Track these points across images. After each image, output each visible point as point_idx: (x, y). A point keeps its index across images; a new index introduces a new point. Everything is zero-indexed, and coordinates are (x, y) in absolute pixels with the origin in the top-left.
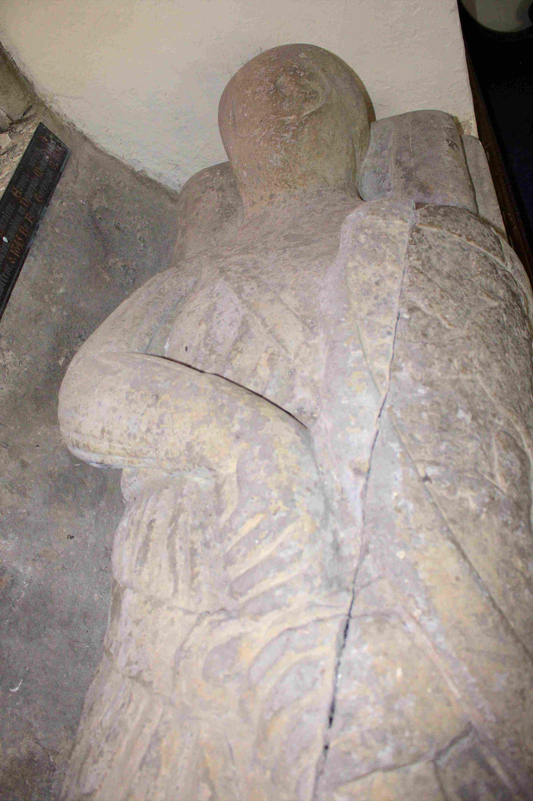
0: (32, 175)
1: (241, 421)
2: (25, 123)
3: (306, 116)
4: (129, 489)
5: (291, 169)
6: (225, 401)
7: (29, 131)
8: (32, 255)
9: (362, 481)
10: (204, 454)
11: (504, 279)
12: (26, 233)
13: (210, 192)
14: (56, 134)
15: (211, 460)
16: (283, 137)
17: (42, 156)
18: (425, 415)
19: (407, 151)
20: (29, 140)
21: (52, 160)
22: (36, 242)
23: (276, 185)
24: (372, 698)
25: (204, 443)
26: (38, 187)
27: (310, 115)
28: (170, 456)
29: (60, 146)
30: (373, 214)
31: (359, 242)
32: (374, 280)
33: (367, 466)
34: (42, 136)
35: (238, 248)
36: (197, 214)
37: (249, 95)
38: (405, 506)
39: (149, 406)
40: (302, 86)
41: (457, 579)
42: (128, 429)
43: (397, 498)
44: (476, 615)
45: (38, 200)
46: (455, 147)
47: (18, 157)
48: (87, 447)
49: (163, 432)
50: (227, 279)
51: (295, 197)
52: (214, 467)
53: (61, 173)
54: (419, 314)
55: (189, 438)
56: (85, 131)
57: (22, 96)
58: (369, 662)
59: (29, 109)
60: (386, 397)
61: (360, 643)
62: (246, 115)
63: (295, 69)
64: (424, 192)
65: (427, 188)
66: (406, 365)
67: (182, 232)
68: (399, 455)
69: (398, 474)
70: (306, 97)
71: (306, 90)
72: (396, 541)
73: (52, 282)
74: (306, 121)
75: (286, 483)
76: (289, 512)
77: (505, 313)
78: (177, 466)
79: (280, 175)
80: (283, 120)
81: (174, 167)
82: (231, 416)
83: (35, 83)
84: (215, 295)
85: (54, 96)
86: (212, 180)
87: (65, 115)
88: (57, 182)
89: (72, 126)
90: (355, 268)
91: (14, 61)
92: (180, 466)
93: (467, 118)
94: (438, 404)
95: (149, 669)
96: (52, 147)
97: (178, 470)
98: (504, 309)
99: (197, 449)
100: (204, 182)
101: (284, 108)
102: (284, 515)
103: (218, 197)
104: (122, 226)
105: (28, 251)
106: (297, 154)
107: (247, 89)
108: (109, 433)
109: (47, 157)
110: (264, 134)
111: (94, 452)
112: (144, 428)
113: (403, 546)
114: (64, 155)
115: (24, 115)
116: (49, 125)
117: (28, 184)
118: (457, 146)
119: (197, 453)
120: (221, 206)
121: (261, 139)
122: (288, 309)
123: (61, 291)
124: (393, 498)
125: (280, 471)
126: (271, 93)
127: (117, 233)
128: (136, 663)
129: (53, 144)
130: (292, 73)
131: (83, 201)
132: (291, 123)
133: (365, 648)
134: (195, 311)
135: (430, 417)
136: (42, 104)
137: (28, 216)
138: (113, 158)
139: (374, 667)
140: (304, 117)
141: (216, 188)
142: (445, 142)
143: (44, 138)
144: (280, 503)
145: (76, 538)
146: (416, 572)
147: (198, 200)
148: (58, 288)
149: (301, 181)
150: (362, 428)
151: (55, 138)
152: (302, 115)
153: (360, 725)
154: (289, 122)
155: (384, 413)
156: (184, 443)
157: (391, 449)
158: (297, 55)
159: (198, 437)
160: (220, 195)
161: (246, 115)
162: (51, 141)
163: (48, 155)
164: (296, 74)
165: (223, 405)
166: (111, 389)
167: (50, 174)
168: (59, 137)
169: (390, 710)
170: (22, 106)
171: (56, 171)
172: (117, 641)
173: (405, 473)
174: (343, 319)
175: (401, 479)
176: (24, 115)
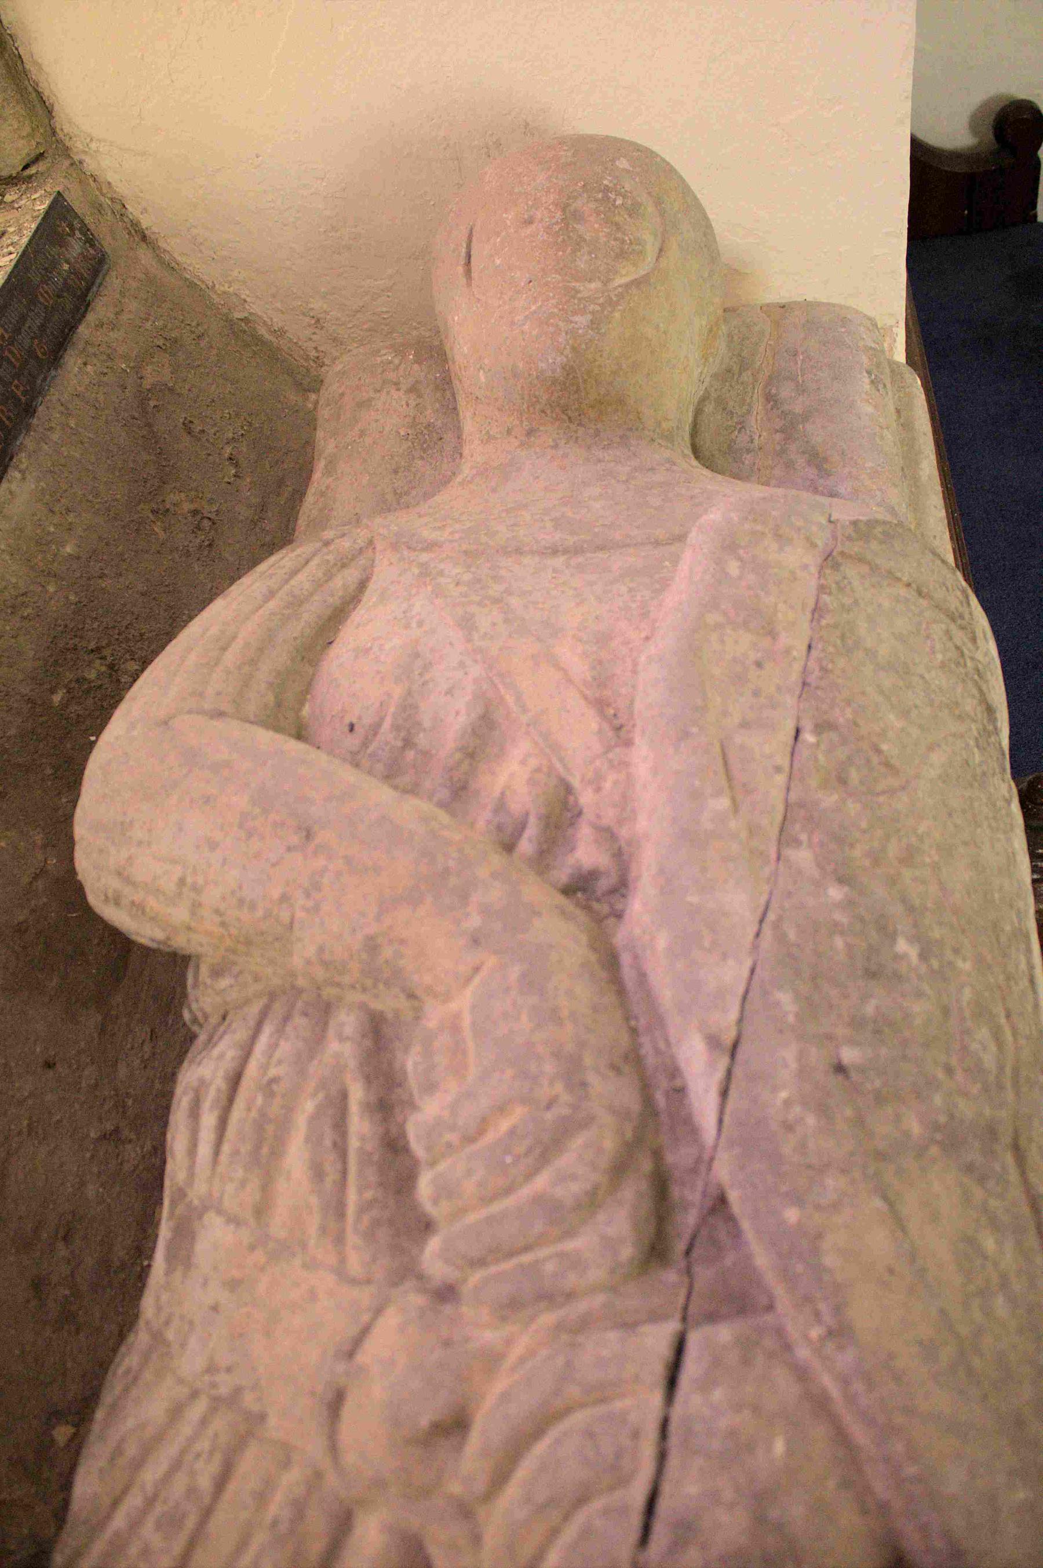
0: (33, 301)
1: (486, 911)
2: (24, 186)
3: (620, 286)
4: (204, 997)
5: (578, 387)
6: (451, 863)
7: (31, 206)
8: (17, 468)
9: (724, 1062)
10: (402, 963)
11: (976, 677)
12: (9, 418)
13: (393, 391)
14: (88, 220)
15: (416, 977)
16: (571, 322)
17: (54, 264)
18: (839, 942)
19: (792, 380)
20: (34, 226)
21: (75, 274)
22: (28, 441)
23: (543, 411)
24: (728, 1495)
25: (402, 942)
26: (43, 327)
27: (627, 286)
28: (327, 957)
29: (92, 246)
30: (755, 521)
31: (727, 574)
32: (753, 656)
33: (732, 1034)
34: (58, 219)
35: (457, 526)
36: (362, 434)
37: (508, 223)
38: (800, 1120)
39: (289, 849)
40: (618, 226)
41: (891, 1271)
42: (240, 887)
43: (787, 1103)
44: (921, 1343)
45: (40, 355)
46: (881, 387)
47: (8, 258)
48: (138, 908)
49: (317, 909)
50: (439, 592)
51: (576, 441)
52: (418, 993)
53: (88, 305)
54: (834, 736)
55: (373, 929)
56: (145, 222)
57: (28, 129)
58: (723, 1423)
59: (39, 157)
60: (770, 899)
61: (705, 1385)
62: (498, 262)
63: (606, 190)
64: (819, 468)
65: (826, 460)
66: (809, 839)
67: (326, 466)
68: (791, 1019)
69: (789, 1054)
70: (622, 250)
71: (624, 234)
72: (784, 1189)
73: (52, 529)
74: (621, 296)
75: (570, 1047)
76: (575, 1108)
77: (978, 747)
78: (338, 979)
79: (556, 395)
80: (574, 289)
81: (313, 322)
82: (464, 897)
83: (56, 108)
84: (414, 625)
85: (92, 140)
86: (397, 368)
87: (109, 183)
88: (80, 321)
89: (118, 207)
90: (719, 626)
91: (20, 57)
92: (346, 980)
93: (891, 322)
94: (862, 920)
95: (255, 1387)
96: (76, 247)
97: (338, 985)
98: (976, 739)
99: (387, 952)
100: (380, 370)
101: (578, 263)
102: (566, 1111)
103: (408, 405)
104: (197, 427)
105: (11, 459)
106: (595, 360)
107: (506, 211)
108: (196, 889)
109: (66, 267)
110: (534, 308)
111: (152, 919)
112: (276, 894)
113: (797, 1199)
114: (98, 265)
115: (25, 168)
116: (75, 200)
117: (23, 318)
118: (885, 386)
119: (387, 962)
120: (413, 424)
121: (526, 317)
122: (570, 681)
123: (69, 549)
124: (779, 1102)
125: (559, 1022)
126: (557, 228)
127: (186, 440)
128: (229, 1370)
129: (80, 239)
130: (600, 196)
131: (128, 366)
132: (589, 297)
133: (718, 1395)
134: (371, 648)
135: (849, 947)
136: (66, 152)
137: (17, 387)
138: (192, 285)
139: (732, 1433)
140: (615, 288)
141: (404, 387)
142: (865, 374)
143: (64, 224)
144: (559, 1087)
145: (61, 1069)
146: (815, 1251)
147: (364, 404)
148: (62, 544)
149: (592, 414)
150: (725, 956)
151: (85, 230)
152: (611, 286)
153: (704, 1547)
154: (585, 294)
155: (767, 932)
156: (360, 936)
157: (778, 1004)
158: (613, 161)
159: (391, 927)
160: (412, 403)
161: (498, 262)
162: (77, 233)
163: (68, 262)
164: (609, 198)
165: (447, 871)
166: (207, 800)
167: (68, 302)
168: (92, 227)
169: (759, 1519)
170: (24, 149)
171: (80, 297)
172: (182, 1318)
173: (801, 1056)
174: (694, 730)
175: (794, 1066)
176: (25, 168)
